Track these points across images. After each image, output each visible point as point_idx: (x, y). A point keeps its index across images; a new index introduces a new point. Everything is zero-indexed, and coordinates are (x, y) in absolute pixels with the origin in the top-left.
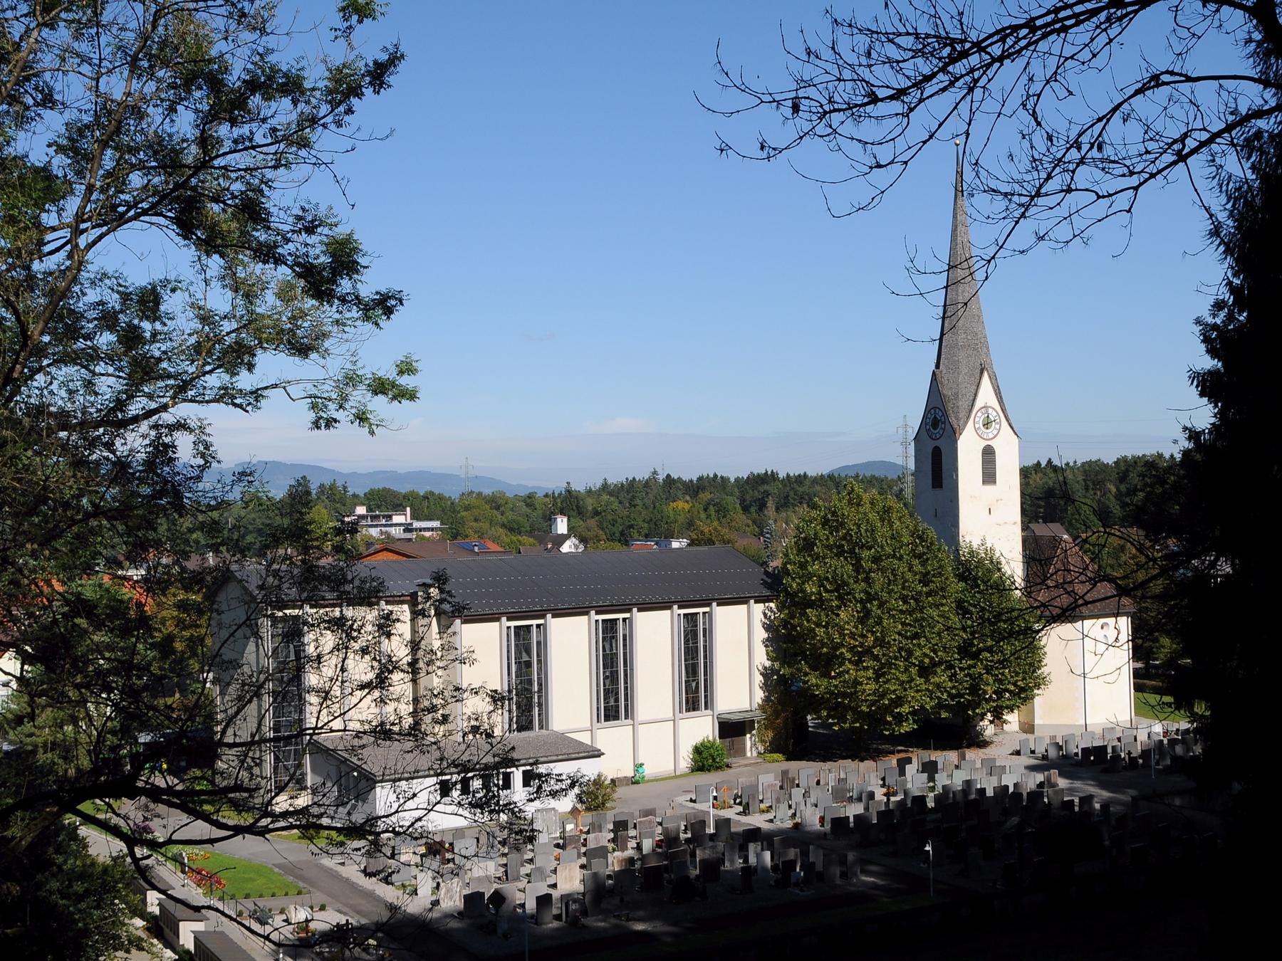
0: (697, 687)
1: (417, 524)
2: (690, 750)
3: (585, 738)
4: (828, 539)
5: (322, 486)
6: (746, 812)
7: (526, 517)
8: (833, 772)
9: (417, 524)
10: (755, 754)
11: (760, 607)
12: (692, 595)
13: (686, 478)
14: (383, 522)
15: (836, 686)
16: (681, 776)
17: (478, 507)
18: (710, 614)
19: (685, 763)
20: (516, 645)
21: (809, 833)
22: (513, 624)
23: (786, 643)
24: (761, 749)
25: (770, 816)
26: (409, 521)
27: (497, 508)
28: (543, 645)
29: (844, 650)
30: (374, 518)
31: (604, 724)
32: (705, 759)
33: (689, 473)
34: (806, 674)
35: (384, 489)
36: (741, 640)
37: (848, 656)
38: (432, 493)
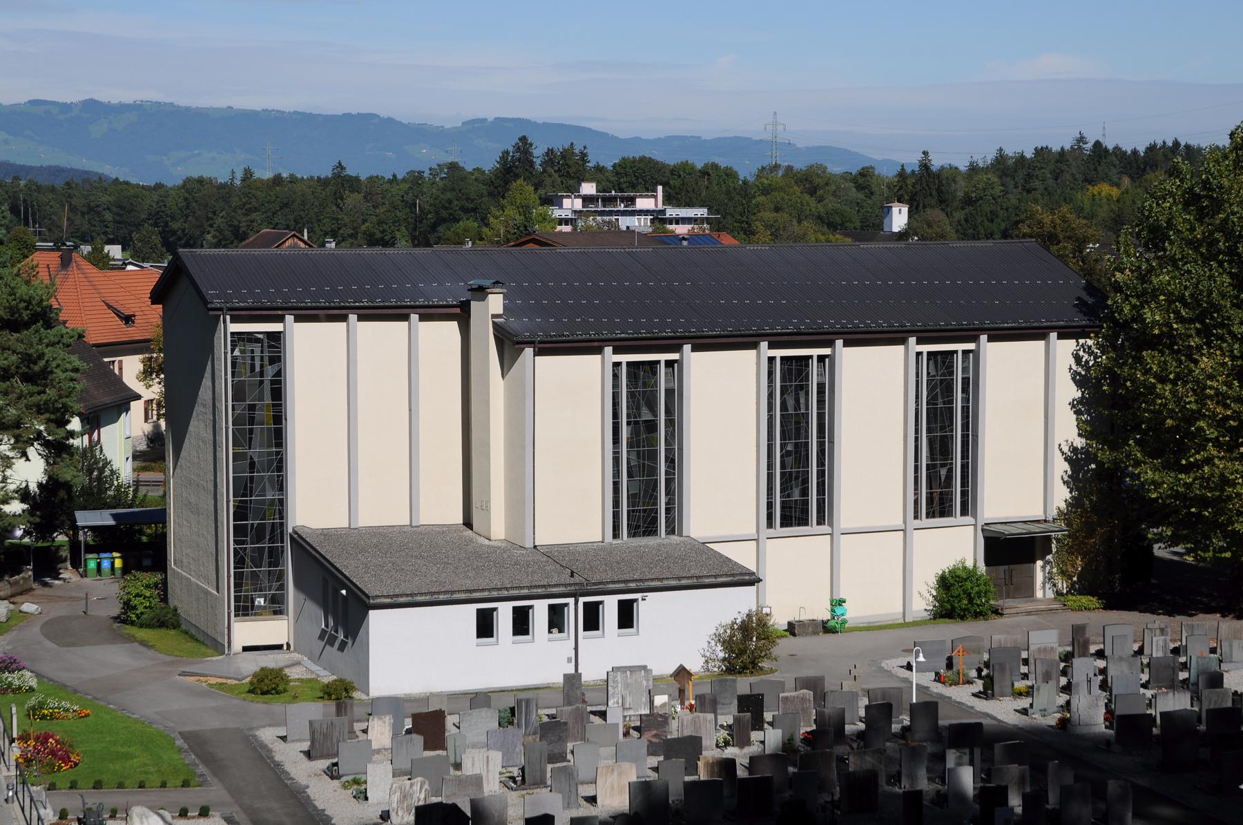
0: (950, 476)
1: (672, 212)
2: (933, 581)
3: (743, 556)
4: (1192, 229)
5: (550, 152)
6: (987, 693)
7: (833, 201)
8: (1158, 633)
9: (672, 212)
10: (1050, 594)
11: (1070, 345)
12: (945, 322)
13: (1128, 148)
14: (622, 207)
15: (1188, 486)
16: (915, 624)
17: (781, 189)
18: (976, 353)
19: (922, 602)
20: (631, 395)
21: (1083, 738)
22: (625, 358)
23: (1108, 406)
24: (1063, 585)
25: (1024, 703)
26: (660, 207)
27: (813, 191)
28: (675, 397)
29: (1202, 424)
30: (608, 201)
31: (779, 530)
32: (956, 597)
33: (1132, 137)
34: (1137, 463)
35: (643, 159)
36: (1030, 402)
37: (1211, 433)
38: (715, 166)
